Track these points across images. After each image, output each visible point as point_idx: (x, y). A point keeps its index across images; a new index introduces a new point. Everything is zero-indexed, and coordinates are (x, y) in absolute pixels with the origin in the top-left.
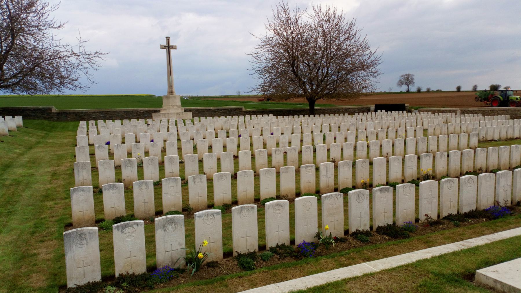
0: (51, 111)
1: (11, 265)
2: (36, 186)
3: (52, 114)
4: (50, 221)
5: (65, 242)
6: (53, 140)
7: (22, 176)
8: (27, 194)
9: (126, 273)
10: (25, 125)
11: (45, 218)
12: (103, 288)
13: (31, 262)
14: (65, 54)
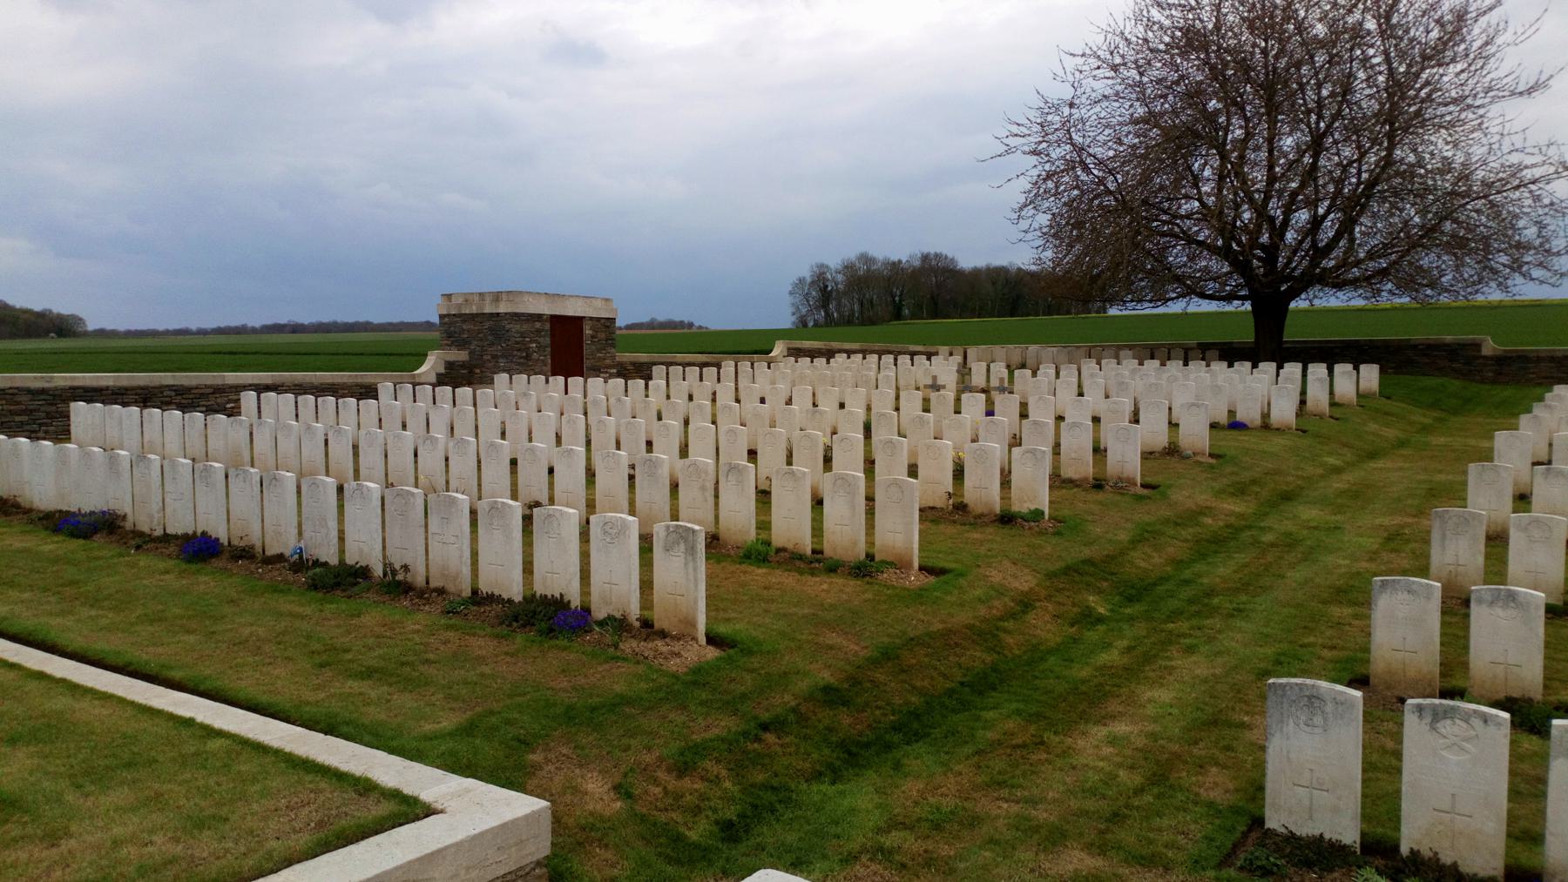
0: (1480, 351)
1: (1177, 730)
2: (1330, 560)
3: (1481, 361)
4: (1319, 658)
5: (1269, 703)
6: (1451, 439)
7: (1309, 528)
8: (1296, 575)
9: (1431, 854)
10: (1385, 392)
11: (1309, 645)
12: (1354, 868)
13: (1223, 738)
14: (1537, 172)
